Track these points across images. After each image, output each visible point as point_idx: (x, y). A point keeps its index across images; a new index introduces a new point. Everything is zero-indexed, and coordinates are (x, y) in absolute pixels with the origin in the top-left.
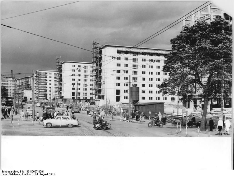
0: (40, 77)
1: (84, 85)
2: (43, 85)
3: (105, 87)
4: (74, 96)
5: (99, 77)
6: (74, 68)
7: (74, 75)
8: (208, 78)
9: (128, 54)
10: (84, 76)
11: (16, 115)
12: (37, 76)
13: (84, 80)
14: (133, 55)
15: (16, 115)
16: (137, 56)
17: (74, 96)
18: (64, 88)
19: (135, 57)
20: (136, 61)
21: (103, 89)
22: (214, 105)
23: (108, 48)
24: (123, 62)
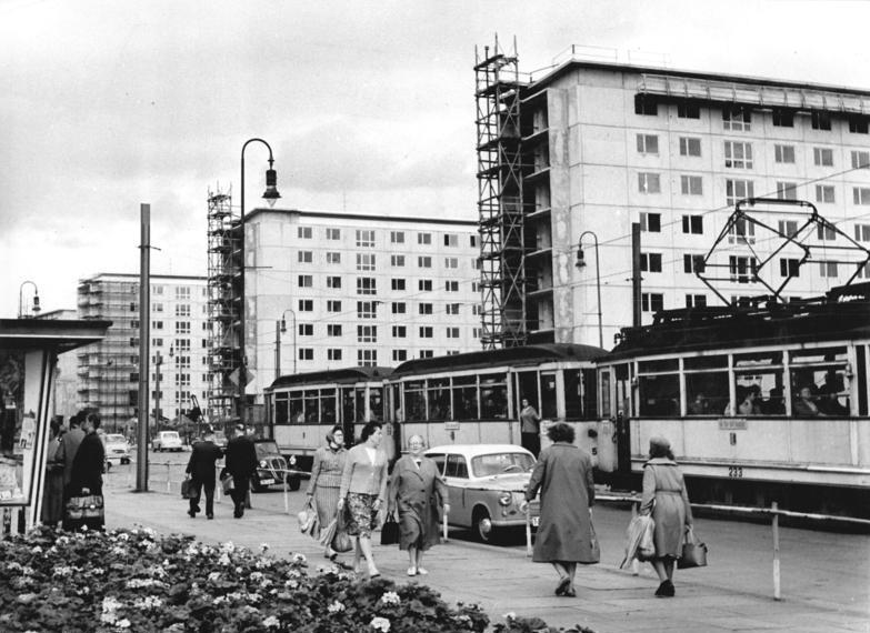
0: (108, 309)
1: (360, 334)
2: (123, 345)
3: (572, 320)
4: (451, 380)
5: (527, 259)
6: (305, 245)
7: (309, 279)
8: (14, 435)
9: (697, 116)
10: (359, 285)
11: (238, 514)
12: (93, 301)
13: (359, 304)
14: (727, 127)
15: (238, 514)
16: (748, 128)
17: (451, 380)
18: (259, 354)
19: (735, 135)
20: (186, 330)
21: (561, 329)
22: (214, 462)
23: (583, 77)
24: (668, 159)
